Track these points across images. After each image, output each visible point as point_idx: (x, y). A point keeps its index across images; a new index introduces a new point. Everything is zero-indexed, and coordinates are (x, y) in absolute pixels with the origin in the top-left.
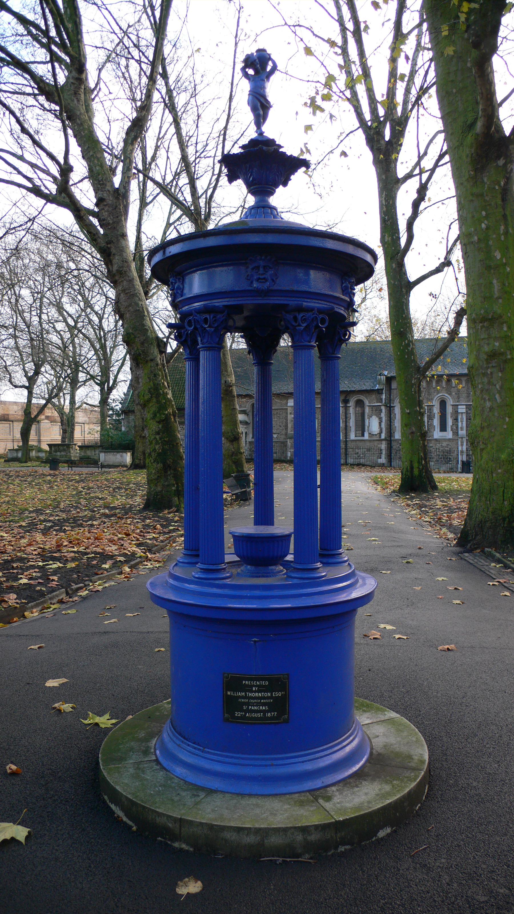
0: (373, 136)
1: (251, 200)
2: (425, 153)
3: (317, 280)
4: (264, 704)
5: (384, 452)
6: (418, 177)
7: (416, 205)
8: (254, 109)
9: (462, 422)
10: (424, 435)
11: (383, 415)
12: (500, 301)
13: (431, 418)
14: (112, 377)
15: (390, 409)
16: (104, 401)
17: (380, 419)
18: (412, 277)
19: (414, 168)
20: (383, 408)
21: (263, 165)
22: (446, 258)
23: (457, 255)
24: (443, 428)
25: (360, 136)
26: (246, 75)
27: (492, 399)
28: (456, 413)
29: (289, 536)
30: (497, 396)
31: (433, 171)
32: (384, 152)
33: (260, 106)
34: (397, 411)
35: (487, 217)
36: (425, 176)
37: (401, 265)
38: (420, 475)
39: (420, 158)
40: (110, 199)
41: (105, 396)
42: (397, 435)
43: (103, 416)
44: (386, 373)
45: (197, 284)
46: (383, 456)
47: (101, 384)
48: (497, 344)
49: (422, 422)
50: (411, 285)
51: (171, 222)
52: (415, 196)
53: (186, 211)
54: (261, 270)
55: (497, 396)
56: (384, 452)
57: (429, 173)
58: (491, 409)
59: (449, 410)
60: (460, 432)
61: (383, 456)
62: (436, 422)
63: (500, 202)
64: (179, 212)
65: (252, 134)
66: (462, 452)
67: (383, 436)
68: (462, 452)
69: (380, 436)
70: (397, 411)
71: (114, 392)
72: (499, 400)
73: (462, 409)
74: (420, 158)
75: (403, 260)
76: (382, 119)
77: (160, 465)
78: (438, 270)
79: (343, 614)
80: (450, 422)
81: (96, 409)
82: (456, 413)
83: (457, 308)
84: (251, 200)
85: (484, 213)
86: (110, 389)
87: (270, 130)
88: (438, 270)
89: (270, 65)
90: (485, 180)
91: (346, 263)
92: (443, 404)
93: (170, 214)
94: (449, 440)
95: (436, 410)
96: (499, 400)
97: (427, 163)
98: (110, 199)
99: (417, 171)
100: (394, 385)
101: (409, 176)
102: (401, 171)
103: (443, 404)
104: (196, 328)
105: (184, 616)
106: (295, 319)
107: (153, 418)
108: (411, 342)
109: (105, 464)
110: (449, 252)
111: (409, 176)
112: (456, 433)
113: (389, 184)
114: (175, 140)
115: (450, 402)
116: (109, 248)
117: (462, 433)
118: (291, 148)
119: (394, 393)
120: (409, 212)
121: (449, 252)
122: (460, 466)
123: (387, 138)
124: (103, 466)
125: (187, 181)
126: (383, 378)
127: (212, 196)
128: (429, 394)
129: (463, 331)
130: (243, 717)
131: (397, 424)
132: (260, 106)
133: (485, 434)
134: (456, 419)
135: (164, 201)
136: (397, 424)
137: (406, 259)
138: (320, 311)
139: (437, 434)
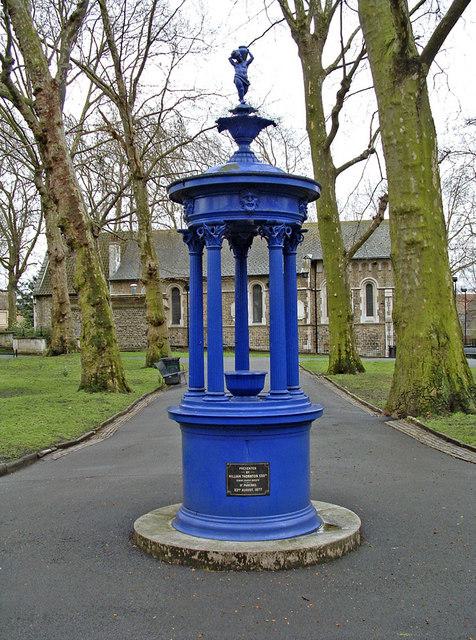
0: (299, 32)
1: (237, 148)
2: (349, 47)
3: (284, 205)
4: (254, 483)
5: (309, 338)
6: (342, 69)
7: (341, 97)
8: (238, 86)
9: (389, 306)
10: (350, 318)
11: (308, 299)
12: (417, 196)
13: (357, 302)
14: (22, 261)
15: (315, 293)
16: (13, 285)
17: (306, 303)
18: (337, 164)
19: (338, 61)
20: (308, 292)
21: (244, 124)
22: (369, 146)
23: (378, 146)
24: (370, 312)
25: (285, 30)
26: (233, 63)
27: (412, 283)
28: (382, 297)
29: (263, 376)
30: (416, 280)
31: (356, 63)
32: (309, 44)
33: (243, 85)
34: (323, 295)
35: (404, 123)
36: (349, 69)
37: (327, 150)
38: (347, 359)
39: (344, 51)
40: (47, 90)
41: (14, 279)
42: (324, 320)
43: (11, 299)
44: (310, 256)
45: (202, 206)
46: (309, 342)
47: (10, 268)
48: (415, 234)
49: (349, 305)
50: (337, 172)
51: (91, 101)
52: (339, 87)
53: (107, 90)
54: (250, 199)
55: (416, 280)
56: (309, 338)
57: (352, 65)
58: (411, 291)
59: (376, 294)
60: (387, 316)
61: (309, 342)
62: (363, 306)
63: (415, 111)
64: (99, 92)
65: (237, 103)
66: (389, 337)
67: (308, 322)
68: (389, 337)
69: (306, 322)
70: (323, 295)
71: (23, 275)
72: (417, 284)
73: (389, 293)
74: (344, 51)
75: (328, 147)
76: (307, 13)
77: (95, 349)
78: (363, 157)
79: (300, 425)
80: (376, 306)
81: (4, 294)
82: (382, 297)
83: (379, 194)
84: (237, 148)
85: (401, 119)
86: (20, 273)
87: (251, 98)
88: (363, 157)
89: (249, 58)
90: (402, 91)
91: (298, 192)
92: (369, 287)
93: (90, 93)
94: (376, 324)
95: (363, 294)
96: (417, 284)
97: (351, 56)
98: (47, 90)
99: (341, 63)
100: (319, 269)
101: (334, 68)
102: (326, 63)
103: (369, 287)
104: (205, 235)
105: (190, 425)
106: (271, 230)
107: (88, 302)
108: (338, 224)
109: (19, 351)
110: (372, 141)
111: (334, 68)
112: (382, 318)
113: (314, 76)
114: (100, 23)
115: (377, 286)
116: (45, 136)
117: (389, 317)
118: (264, 114)
119: (319, 276)
120: (334, 102)
121: (372, 141)
122: (387, 351)
123: (312, 31)
124: (17, 354)
125: (113, 63)
126: (308, 262)
127: (137, 80)
128: (355, 278)
129: (386, 216)
130: (240, 492)
131: (323, 308)
132: (243, 85)
133: (406, 314)
134: (383, 304)
135: (84, 81)
136: (323, 308)
137: (331, 146)
138: (287, 225)
139: (364, 319)
